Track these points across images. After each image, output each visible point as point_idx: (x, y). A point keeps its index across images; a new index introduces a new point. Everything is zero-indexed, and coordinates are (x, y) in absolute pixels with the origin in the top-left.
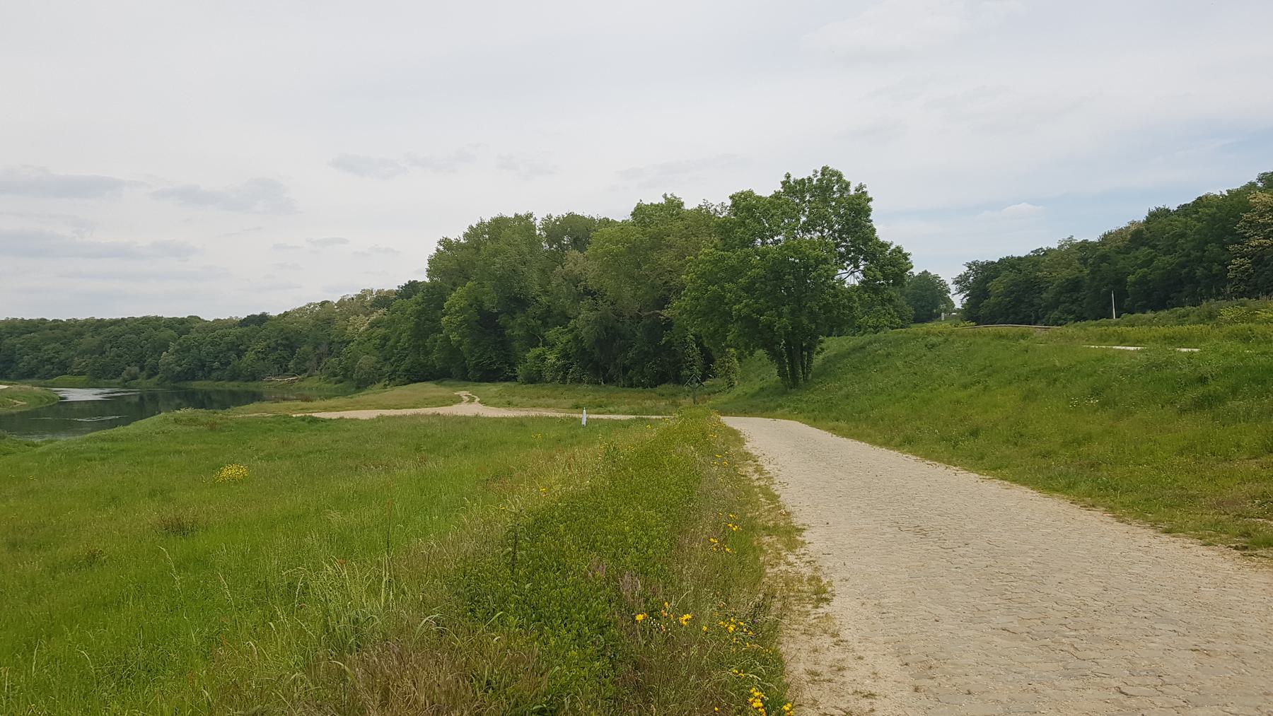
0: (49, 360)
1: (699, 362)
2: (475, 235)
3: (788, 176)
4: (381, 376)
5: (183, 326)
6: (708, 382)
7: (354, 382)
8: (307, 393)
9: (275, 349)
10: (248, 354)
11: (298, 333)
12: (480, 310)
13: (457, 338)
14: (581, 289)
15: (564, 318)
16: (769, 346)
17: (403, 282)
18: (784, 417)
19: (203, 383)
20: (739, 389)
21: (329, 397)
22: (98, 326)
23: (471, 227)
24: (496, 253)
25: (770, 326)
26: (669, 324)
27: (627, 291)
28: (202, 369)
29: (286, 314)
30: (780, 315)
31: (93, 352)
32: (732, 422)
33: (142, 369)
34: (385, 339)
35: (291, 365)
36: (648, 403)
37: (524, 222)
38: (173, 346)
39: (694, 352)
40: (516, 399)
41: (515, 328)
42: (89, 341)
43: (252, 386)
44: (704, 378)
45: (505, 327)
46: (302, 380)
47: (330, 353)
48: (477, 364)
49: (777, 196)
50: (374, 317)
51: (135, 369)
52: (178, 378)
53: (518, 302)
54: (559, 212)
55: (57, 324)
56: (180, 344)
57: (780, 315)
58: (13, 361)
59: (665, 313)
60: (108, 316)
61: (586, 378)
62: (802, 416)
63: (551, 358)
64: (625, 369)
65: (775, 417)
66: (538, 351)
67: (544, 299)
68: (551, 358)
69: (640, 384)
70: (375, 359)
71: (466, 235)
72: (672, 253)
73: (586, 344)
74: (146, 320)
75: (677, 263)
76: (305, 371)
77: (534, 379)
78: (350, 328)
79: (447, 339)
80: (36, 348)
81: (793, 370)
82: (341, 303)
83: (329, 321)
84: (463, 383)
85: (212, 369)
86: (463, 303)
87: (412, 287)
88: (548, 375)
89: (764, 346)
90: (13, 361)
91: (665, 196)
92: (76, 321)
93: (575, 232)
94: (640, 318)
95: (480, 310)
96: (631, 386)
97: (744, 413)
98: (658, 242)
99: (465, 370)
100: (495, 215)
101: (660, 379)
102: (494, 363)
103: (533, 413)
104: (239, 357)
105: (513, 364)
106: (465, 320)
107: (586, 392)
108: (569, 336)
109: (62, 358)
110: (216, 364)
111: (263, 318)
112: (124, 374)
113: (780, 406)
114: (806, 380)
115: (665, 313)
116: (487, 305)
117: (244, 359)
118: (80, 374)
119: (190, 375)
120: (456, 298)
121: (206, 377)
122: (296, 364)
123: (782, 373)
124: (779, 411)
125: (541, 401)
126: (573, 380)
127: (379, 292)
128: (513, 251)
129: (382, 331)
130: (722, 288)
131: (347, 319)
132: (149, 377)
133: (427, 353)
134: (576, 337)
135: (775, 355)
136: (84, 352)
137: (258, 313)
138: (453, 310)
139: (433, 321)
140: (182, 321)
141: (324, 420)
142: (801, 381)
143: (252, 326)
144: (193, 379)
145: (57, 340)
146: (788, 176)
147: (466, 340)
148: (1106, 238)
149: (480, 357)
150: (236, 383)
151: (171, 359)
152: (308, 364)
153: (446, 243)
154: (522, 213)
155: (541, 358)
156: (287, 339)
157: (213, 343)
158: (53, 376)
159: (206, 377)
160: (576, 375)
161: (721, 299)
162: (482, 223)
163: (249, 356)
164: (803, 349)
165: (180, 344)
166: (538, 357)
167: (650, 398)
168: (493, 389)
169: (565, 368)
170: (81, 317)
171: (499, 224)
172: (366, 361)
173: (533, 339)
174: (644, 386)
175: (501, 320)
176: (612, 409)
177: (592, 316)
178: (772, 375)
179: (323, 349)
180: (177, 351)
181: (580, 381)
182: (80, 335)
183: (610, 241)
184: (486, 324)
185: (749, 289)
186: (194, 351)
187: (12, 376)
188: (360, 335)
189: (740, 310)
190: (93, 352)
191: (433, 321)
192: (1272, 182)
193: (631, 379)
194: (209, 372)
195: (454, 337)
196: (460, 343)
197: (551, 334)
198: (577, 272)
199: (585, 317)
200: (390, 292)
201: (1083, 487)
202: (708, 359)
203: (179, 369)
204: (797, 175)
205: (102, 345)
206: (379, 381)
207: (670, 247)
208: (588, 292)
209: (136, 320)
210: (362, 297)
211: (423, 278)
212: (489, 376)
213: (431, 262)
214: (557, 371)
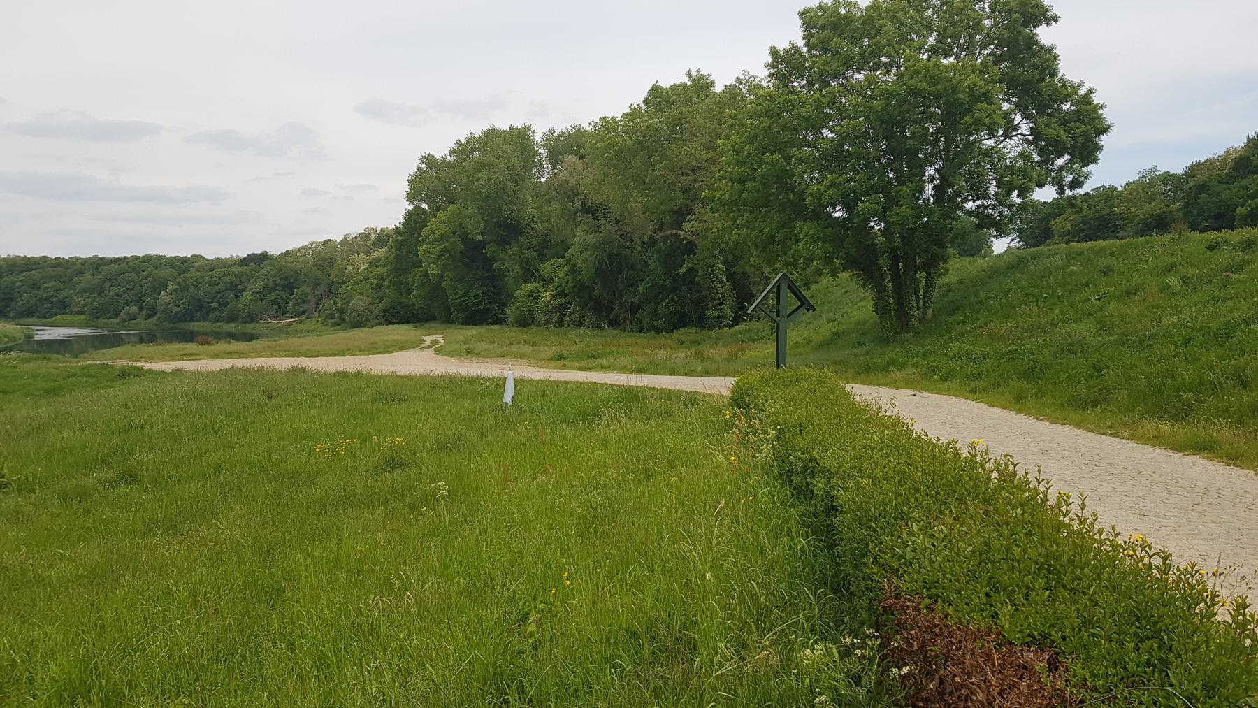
0: (48, 299)
1: (731, 299)
2: (462, 150)
5: (182, 265)
6: (742, 326)
9: (273, 289)
10: (245, 294)
11: (298, 272)
13: (437, 272)
19: (202, 324)
22: (98, 264)
23: (459, 143)
26: (691, 248)
27: (637, 203)
28: (198, 310)
29: (288, 252)
31: (93, 291)
33: (141, 309)
36: (661, 354)
38: (171, 286)
39: (725, 287)
41: (508, 261)
42: (89, 278)
43: (249, 328)
44: (736, 321)
45: (493, 260)
46: (300, 322)
47: (329, 293)
48: (461, 304)
51: (134, 309)
53: (510, 230)
55: (58, 263)
56: (178, 284)
58: (12, 299)
61: (586, 322)
62: (953, 383)
63: (546, 296)
66: (530, 287)
67: (540, 227)
68: (546, 296)
71: (452, 152)
72: (697, 142)
74: (148, 259)
75: (705, 155)
76: (303, 313)
77: (525, 322)
78: (350, 268)
79: (426, 274)
80: (36, 286)
82: (344, 242)
83: (330, 261)
85: (210, 310)
88: (541, 318)
90: (12, 299)
91: (689, 75)
92: (78, 258)
95: (465, 239)
96: (641, 330)
101: (679, 321)
103: (226, 364)
104: (237, 297)
105: (505, 305)
106: (446, 251)
107: (584, 338)
108: (567, 268)
109: (61, 297)
110: (214, 305)
111: (263, 258)
112: (122, 314)
113: (894, 363)
116: (470, 229)
117: (242, 299)
118: (80, 313)
119: (188, 316)
121: (204, 318)
122: (294, 305)
123: (880, 308)
124: (897, 374)
125: (514, 348)
126: (571, 323)
128: (502, 164)
129: (381, 270)
130: (788, 158)
132: (149, 317)
136: (84, 291)
137: (259, 252)
138: (432, 237)
140: (184, 260)
142: (914, 321)
143: (252, 265)
144: (192, 320)
145: (54, 278)
147: (448, 275)
148: (1193, 170)
149: (465, 294)
150: (233, 325)
151: (168, 298)
152: (306, 305)
153: (429, 160)
154: (519, 125)
155: (534, 296)
156: (286, 279)
157: (211, 283)
158: (52, 315)
159: (204, 318)
160: (576, 317)
163: (247, 296)
165: (178, 284)
166: (530, 295)
167: (663, 347)
169: (563, 308)
170: (84, 255)
172: (359, 302)
174: (657, 331)
175: (490, 250)
176: (604, 362)
177: (593, 238)
179: (322, 290)
180: (175, 291)
181: (580, 324)
182: (80, 273)
184: (472, 255)
186: (193, 290)
187: (12, 314)
190: (93, 291)
192: (1256, 144)
194: (208, 313)
195: (433, 270)
196: (442, 277)
197: (546, 267)
198: (573, 181)
201: (586, 321)
203: (177, 309)
205: (101, 283)
208: (586, 209)
209: (137, 258)
210: (365, 236)
212: (476, 316)
213: (411, 182)
214: (552, 312)
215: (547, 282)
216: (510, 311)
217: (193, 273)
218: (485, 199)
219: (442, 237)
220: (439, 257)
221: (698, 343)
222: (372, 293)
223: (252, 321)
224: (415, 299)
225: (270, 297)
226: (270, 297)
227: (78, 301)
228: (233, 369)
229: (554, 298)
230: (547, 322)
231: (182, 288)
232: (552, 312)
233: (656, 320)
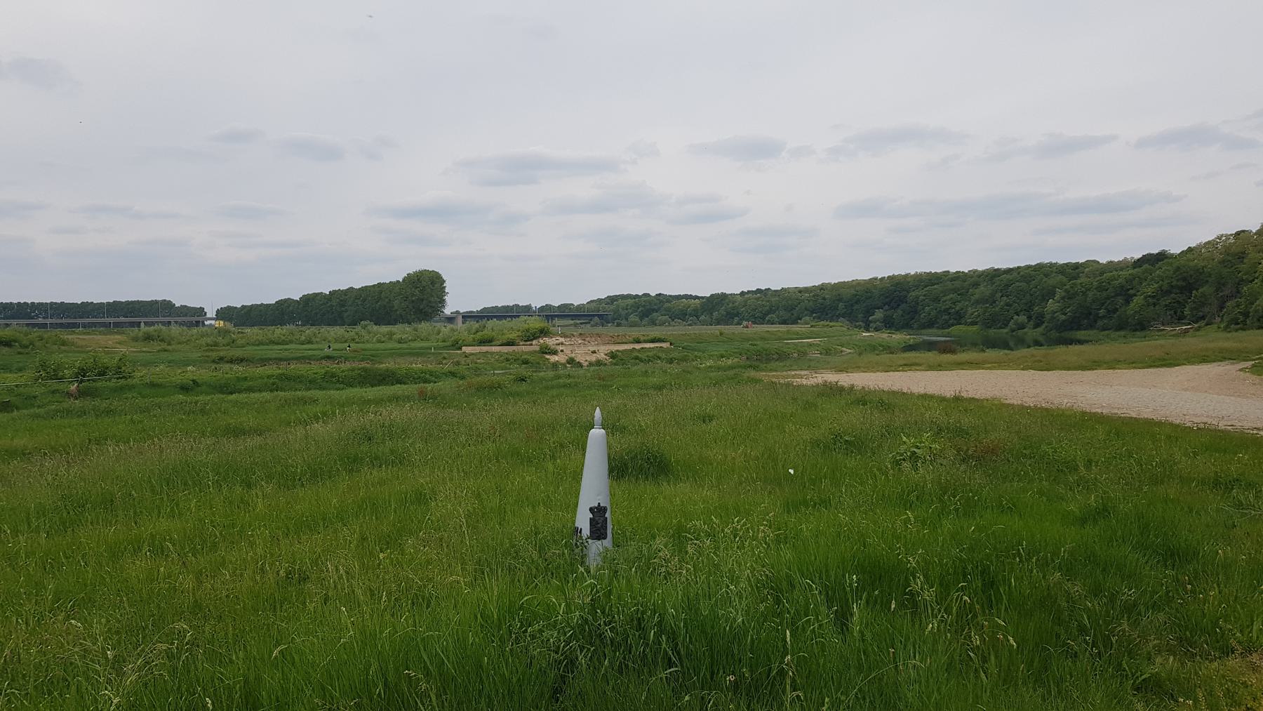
0: (946, 311)
9: (1168, 292)
33: (1030, 318)
38: (1059, 293)
42: (984, 290)
51: (1022, 318)
55: (959, 276)
74: (1039, 267)
80: (937, 300)
85: (1097, 318)
111: (1162, 256)
122: (1192, 309)
132: (1037, 326)
145: (955, 291)
152: (1206, 309)
158: (949, 326)
170: (981, 267)
182: (976, 285)
227: (972, 312)
231: (1070, 296)
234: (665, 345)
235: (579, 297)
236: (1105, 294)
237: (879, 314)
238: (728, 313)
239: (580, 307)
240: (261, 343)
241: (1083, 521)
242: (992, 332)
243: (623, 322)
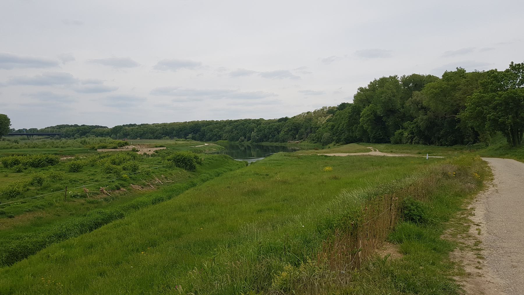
0: (216, 135)
2: (373, 86)
3: (512, 63)
4: (333, 140)
5: (258, 122)
7: (323, 143)
8: (303, 147)
9: (291, 130)
11: (299, 124)
12: (375, 115)
14: (419, 107)
15: (412, 118)
16: (503, 130)
17: (340, 103)
18: (508, 158)
20: (490, 147)
21: (160, 138)
22: (230, 122)
23: (371, 82)
24: (382, 93)
25: (503, 123)
26: (459, 121)
30: (508, 118)
32: (484, 159)
33: (245, 138)
34: (333, 126)
35: (297, 136)
37: (393, 79)
38: (255, 130)
40: (394, 150)
41: (390, 122)
42: (228, 128)
43: (283, 144)
44: (475, 142)
46: (301, 142)
47: (311, 132)
48: (374, 136)
49: (507, 71)
50: (328, 118)
51: (243, 138)
52: (258, 141)
53: (391, 111)
54: (408, 73)
55: (217, 122)
57: (508, 118)
59: (457, 116)
60: (233, 119)
61: (421, 142)
63: (406, 134)
64: (439, 139)
65: (504, 158)
66: (400, 131)
67: (402, 110)
69: (445, 145)
70: (329, 134)
71: (369, 86)
72: (461, 92)
73: (422, 129)
74: (246, 120)
77: (399, 142)
78: (319, 122)
79: (362, 127)
80: (211, 131)
81: (514, 140)
82: (315, 112)
83: (310, 119)
84: (368, 144)
85: (269, 138)
86: (369, 113)
87: (343, 106)
88: (404, 141)
89: (501, 130)
91: (457, 68)
93: (416, 82)
94: (445, 118)
95: (375, 115)
96: (442, 145)
97: (492, 156)
98: (454, 88)
99: (369, 139)
100: (381, 77)
101: (454, 143)
102: (381, 136)
103: (406, 155)
104: (278, 134)
111: (286, 119)
113: (507, 154)
114: (519, 143)
115: (457, 116)
116: (378, 113)
118: (226, 139)
119: (261, 140)
120: (365, 111)
122: (299, 136)
123: (509, 141)
124: (506, 156)
125: (405, 151)
127: (329, 107)
129: (331, 123)
131: (317, 118)
132: (248, 141)
133: (353, 132)
134: (417, 126)
135: (506, 134)
136: (226, 132)
137: (284, 117)
139: (355, 119)
140: (258, 120)
141: (329, 156)
143: (283, 122)
145: (217, 128)
146: (512, 63)
147: (370, 127)
149: (375, 134)
150: (277, 143)
151: (255, 134)
152: (303, 136)
153: (361, 89)
154: (393, 75)
155: (402, 134)
157: (269, 128)
158: (217, 141)
160: (417, 141)
161: (482, 112)
162: (376, 80)
164: (518, 131)
168: (382, 146)
170: (225, 119)
171: (383, 81)
172: (326, 135)
173: (397, 126)
175: (384, 119)
177: (425, 117)
178: (504, 141)
179: (309, 130)
181: (418, 143)
182: (225, 126)
183: (433, 88)
184: (377, 120)
185: (495, 108)
188: (323, 125)
189: (490, 117)
191: (355, 119)
193: (441, 142)
195: (365, 126)
197: (406, 124)
198: (418, 100)
199: (421, 119)
200: (334, 107)
202: (476, 134)
204: (516, 62)
205: (232, 129)
206: (331, 143)
207: (460, 90)
208: (423, 108)
211: (351, 101)
213: (355, 97)
214: (408, 139)
215: (406, 129)
216: (392, 139)
217: (262, 125)
218: (383, 103)
219: (368, 115)
220: (367, 121)
221: (462, 149)
222: (330, 131)
223: (284, 142)
224: (357, 134)
225: (290, 133)
226: (290, 133)
227: (225, 135)
228: (364, 155)
229: (409, 134)
230: (407, 143)
231: (260, 131)
232: (408, 139)
233: (447, 142)
234: (165, 148)
235: (40, 126)
236: (271, 130)
237: (190, 136)
238: (124, 134)
239: (42, 130)
240: (7, 148)
241: (496, 150)
242: (233, 143)
243: (72, 137)
